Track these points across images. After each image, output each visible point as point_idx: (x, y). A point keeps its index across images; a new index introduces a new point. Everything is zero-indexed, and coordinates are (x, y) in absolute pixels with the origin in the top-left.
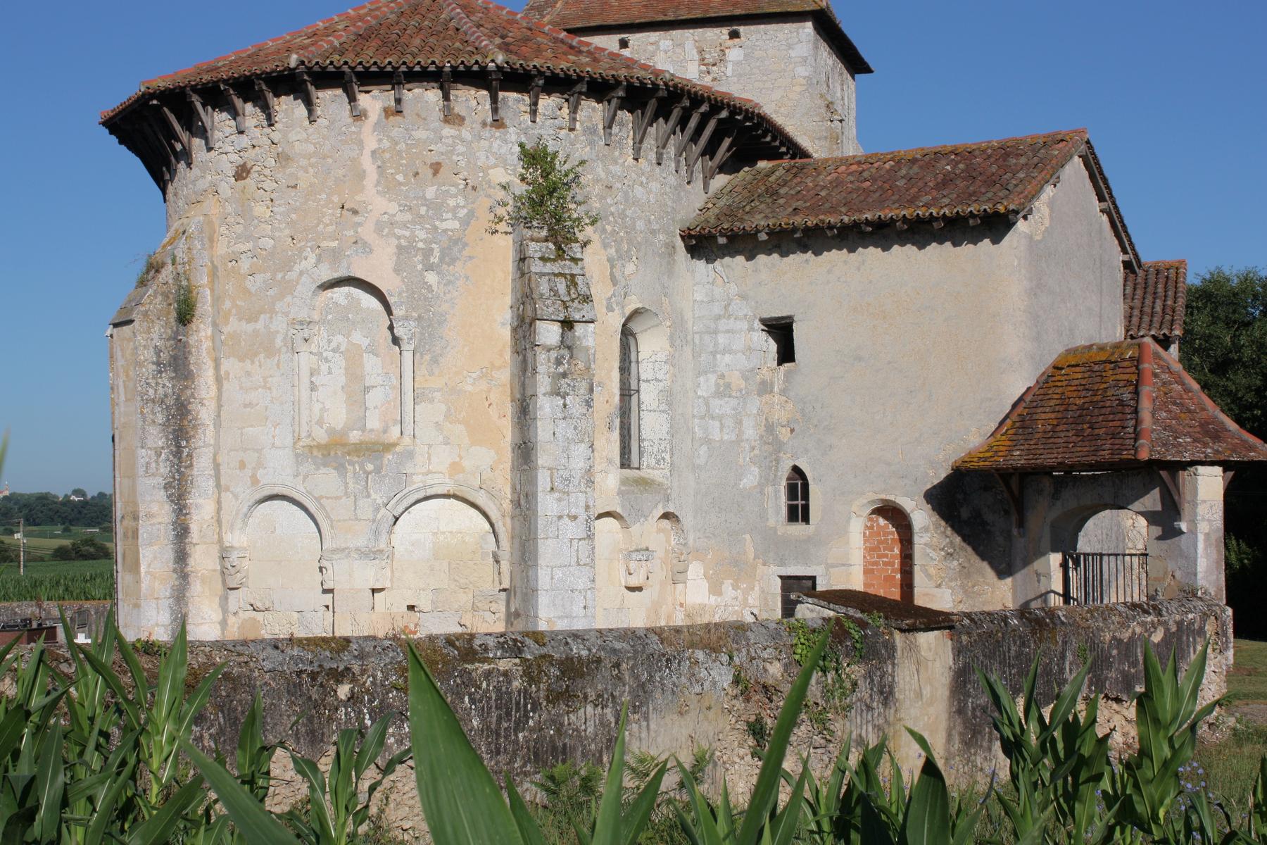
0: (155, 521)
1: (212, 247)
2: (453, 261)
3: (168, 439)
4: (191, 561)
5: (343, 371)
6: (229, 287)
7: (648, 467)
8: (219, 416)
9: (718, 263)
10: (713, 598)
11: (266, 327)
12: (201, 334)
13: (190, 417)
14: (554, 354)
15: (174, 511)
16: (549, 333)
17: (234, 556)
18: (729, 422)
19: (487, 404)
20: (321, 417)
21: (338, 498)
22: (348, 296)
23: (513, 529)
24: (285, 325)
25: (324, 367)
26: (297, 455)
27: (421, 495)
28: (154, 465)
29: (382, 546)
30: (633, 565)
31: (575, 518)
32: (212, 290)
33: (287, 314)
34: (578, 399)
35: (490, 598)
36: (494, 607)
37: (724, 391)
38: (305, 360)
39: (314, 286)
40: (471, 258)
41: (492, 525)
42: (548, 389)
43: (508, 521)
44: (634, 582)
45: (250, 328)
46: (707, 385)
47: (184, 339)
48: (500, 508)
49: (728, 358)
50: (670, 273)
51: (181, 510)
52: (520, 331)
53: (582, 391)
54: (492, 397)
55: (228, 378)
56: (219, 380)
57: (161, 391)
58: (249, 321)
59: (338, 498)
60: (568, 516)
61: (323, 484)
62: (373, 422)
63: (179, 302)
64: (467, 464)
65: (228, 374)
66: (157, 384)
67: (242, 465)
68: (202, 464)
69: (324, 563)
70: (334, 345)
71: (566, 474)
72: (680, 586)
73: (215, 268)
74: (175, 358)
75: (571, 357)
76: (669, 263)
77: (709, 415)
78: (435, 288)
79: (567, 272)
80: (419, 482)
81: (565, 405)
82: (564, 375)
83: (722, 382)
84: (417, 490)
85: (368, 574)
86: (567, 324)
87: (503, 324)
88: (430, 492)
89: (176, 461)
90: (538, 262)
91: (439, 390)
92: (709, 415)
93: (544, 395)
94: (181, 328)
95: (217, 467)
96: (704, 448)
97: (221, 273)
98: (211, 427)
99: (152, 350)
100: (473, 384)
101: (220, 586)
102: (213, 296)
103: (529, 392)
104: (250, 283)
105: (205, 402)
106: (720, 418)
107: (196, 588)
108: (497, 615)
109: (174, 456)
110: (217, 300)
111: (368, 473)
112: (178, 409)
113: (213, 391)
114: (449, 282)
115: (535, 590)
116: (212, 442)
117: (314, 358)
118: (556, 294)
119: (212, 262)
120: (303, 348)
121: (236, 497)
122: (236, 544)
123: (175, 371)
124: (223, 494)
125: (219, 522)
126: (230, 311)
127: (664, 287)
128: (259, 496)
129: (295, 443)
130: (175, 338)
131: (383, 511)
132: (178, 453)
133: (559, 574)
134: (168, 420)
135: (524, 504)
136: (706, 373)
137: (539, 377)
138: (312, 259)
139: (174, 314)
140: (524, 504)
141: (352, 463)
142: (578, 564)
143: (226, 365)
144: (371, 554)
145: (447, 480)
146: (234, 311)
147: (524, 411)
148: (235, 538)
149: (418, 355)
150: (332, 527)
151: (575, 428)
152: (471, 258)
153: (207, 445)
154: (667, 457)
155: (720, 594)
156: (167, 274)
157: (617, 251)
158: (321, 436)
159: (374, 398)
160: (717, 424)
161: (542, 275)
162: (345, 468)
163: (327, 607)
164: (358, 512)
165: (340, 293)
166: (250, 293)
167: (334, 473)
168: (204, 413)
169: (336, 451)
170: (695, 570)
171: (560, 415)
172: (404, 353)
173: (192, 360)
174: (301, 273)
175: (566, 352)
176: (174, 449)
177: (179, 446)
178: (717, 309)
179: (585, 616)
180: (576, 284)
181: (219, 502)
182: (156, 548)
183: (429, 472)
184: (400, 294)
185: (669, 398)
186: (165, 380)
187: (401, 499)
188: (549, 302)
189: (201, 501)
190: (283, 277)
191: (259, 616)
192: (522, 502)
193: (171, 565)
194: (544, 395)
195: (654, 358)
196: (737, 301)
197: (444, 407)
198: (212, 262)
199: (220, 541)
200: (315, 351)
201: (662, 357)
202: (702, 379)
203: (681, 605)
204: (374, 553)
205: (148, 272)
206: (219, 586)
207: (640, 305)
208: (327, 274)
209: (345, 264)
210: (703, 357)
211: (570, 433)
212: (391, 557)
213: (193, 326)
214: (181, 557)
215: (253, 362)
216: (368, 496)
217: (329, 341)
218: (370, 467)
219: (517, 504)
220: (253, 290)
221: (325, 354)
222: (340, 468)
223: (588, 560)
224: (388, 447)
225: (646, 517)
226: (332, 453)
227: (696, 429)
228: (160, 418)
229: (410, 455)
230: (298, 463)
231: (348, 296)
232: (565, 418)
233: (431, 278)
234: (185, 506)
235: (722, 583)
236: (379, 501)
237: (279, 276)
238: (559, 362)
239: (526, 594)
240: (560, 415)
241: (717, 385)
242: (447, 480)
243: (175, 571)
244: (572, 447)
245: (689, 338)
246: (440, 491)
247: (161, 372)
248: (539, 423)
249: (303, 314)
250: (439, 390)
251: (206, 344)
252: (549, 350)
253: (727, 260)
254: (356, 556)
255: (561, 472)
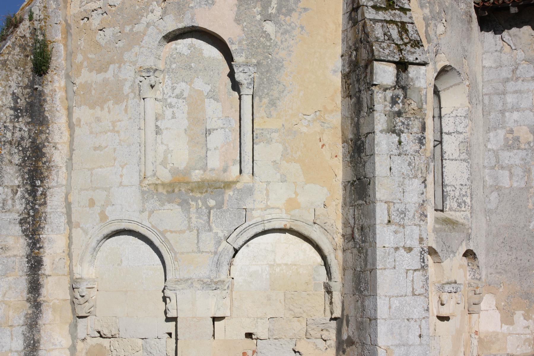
0: (9, 253)
1: (66, 7)
2: (289, 12)
3: (23, 177)
4: (43, 291)
5: (185, 115)
6: (82, 43)
7: (451, 209)
8: (71, 159)
9: (505, 34)
10: (505, 327)
11: (115, 75)
12: (55, 85)
13: (44, 159)
14: (389, 94)
15: (29, 245)
16: (385, 74)
17: (83, 288)
18: (519, 171)
19: (320, 144)
20: (165, 158)
21: (182, 232)
22: (191, 46)
23: (345, 261)
24: (132, 74)
25: (168, 112)
26: (143, 193)
27: (259, 229)
28: (10, 202)
29: (223, 276)
30: (445, 297)
31: (410, 249)
32: (66, 46)
33: (134, 63)
34: (411, 137)
35: (322, 327)
36: (325, 335)
37: (513, 143)
38: (151, 107)
39: (160, 36)
40: (305, 9)
41: (324, 258)
42: (385, 126)
43: (340, 253)
44: (444, 312)
45: (100, 77)
46: (497, 139)
47: (40, 88)
48: (332, 241)
49: (516, 115)
50: (469, 39)
51: (35, 244)
52: (353, 76)
53: (415, 130)
54: (325, 139)
55: (79, 125)
56: (71, 127)
57: (18, 134)
58: (99, 71)
59: (182, 232)
60: (404, 247)
61: (168, 220)
62: (214, 162)
63: (35, 54)
64: (302, 199)
65: (79, 120)
66: (14, 127)
67: (92, 203)
68: (54, 203)
69: (168, 293)
70: (177, 91)
71: (402, 207)
72: (474, 316)
73: (68, 26)
74: (31, 105)
75: (405, 97)
76: (468, 30)
77: (499, 165)
78: (273, 36)
79: (398, 20)
80: (259, 217)
81: (400, 143)
82: (399, 114)
83: (510, 136)
84: (256, 224)
85: (210, 304)
86: (402, 66)
87: (335, 71)
88: (268, 226)
89: (31, 199)
90: (371, 10)
91: (276, 131)
92: (499, 165)
93: (381, 132)
94: (37, 78)
95: (68, 205)
96: (495, 195)
97: (74, 30)
98: (64, 169)
99: (10, 97)
100: (308, 126)
101: (70, 315)
102: (66, 50)
103: (364, 130)
104: (100, 37)
105: (58, 146)
106: (510, 168)
107: (48, 316)
108: (328, 342)
109: (30, 194)
110: (70, 55)
111: (210, 209)
112: (33, 152)
113: (66, 137)
114: (286, 32)
115: (373, 319)
116: (64, 182)
117: (159, 105)
118: (390, 38)
119: (66, 21)
120: (149, 93)
121: (86, 232)
122: (85, 276)
123: (31, 116)
124: (74, 230)
125: (70, 255)
126: (82, 63)
127: (465, 50)
128: (108, 230)
129: (141, 182)
130: (31, 87)
131: (224, 243)
132: (33, 192)
133: (396, 303)
134: (24, 161)
135: (359, 238)
136: (495, 129)
137: (376, 115)
138: (158, 11)
139: (30, 65)
140: (359, 238)
141: (195, 199)
142: (414, 295)
143: (77, 113)
144: (213, 285)
145: (284, 215)
146: (85, 64)
147: (358, 149)
148: (85, 271)
149: (256, 99)
150: (176, 259)
151: (410, 164)
152: (305, 9)
153: (59, 186)
154: (468, 200)
155: (512, 323)
156: (24, 28)
157: (431, 12)
158: (165, 176)
159: (215, 140)
160: (506, 173)
161: (376, 21)
162: (188, 203)
163: (170, 334)
164: (201, 244)
165: (184, 45)
166: (100, 46)
167: (177, 209)
168: (57, 156)
169: (180, 189)
170: (488, 302)
171: (396, 152)
172: (244, 97)
173: (47, 107)
174: (148, 25)
175: (400, 92)
176: (29, 187)
177: (33, 185)
178: (505, 73)
179: (421, 344)
180: (406, 31)
181: (70, 238)
182: (11, 278)
183: (267, 208)
184: (240, 42)
185: (467, 148)
186: (21, 124)
187: (241, 233)
188: (384, 45)
189: (53, 236)
190: (131, 30)
191: (105, 342)
192: (357, 235)
193: (25, 295)
194: (381, 132)
195: (454, 114)
196: (525, 65)
197: (281, 147)
198: (66, 21)
199: (71, 272)
200: (160, 97)
201: (462, 112)
202: (491, 134)
203: (476, 333)
204: (216, 283)
205: (8, 28)
206: (69, 315)
207: (447, 63)
208: (172, 24)
209: (189, 15)
210: (493, 115)
211: (405, 169)
212: (231, 288)
213: (48, 77)
214: (35, 287)
215: (102, 109)
216: (210, 230)
217: (173, 89)
218: (212, 203)
219: (349, 237)
220: (103, 42)
221: (169, 100)
222: (184, 204)
223: (423, 291)
224: (228, 185)
225: (454, 253)
226: (176, 190)
227: (487, 178)
228: (17, 159)
229: (250, 191)
230: (144, 200)
231: (191, 46)
232: (399, 155)
233: (269, 27)
234: (39, 241)
235: (513, 314)
236: (221, 234)
237: (128, 29)
238: (394, 101)
239: (362, 323)
240: (396, 152)
241: (506, 139)
242: (284, 215)
243: (28, 300)
244: (407, 181)
245: (481, 98)
246: (277, 226)
247: (17, 117)
248: (377, 159)
249: (150, 63)
250: (276, 131)
251: (60, 94)
252: (385, 90)
253: (514, 30)
254: (199, 286)
255: (397, 206)
